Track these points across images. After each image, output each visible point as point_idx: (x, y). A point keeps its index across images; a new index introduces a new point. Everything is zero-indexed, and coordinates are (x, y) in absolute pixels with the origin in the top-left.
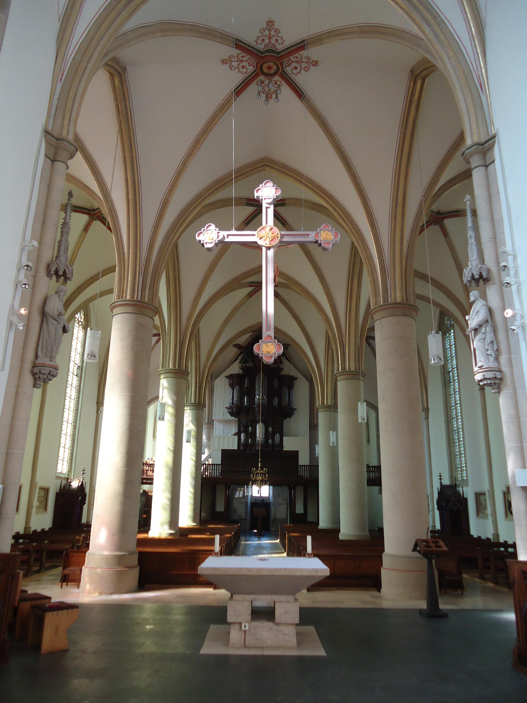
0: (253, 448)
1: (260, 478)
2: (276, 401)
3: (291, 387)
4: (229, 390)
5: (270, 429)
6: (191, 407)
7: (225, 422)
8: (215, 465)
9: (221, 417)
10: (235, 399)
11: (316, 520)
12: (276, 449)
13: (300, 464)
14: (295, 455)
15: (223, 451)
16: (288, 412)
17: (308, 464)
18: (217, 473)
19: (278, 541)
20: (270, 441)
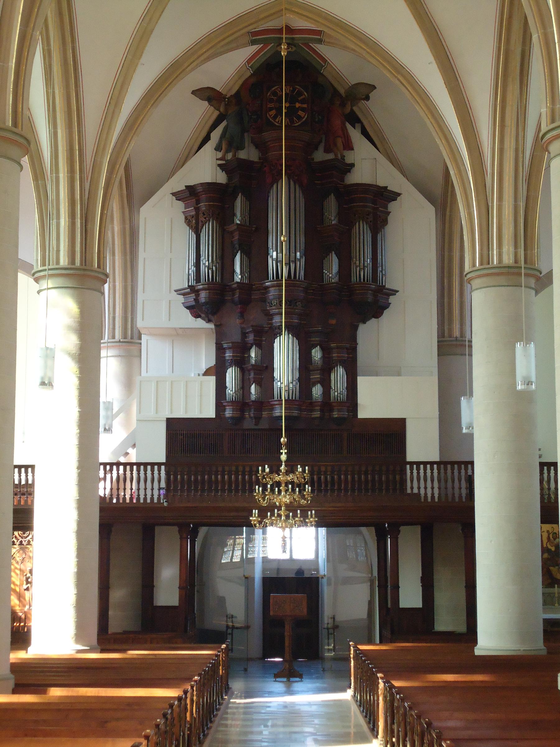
0: (265, 414)
1: (286, 499)
2: (332, 268)
3: (378, 223)
4: (184, 236)
5: (317, 354)
6: (59, 281)
7: (178, 335)
8: (145, 465)
9: (163, 322)
10: (205, 262)
11: (462, 628)
12: (335, 415)
14: (392, 433)
15: (171, 423)
16: (372, 300)
17: (437, 459)
18: (154, 490)
19: (348, 695)
20: (317, 391)
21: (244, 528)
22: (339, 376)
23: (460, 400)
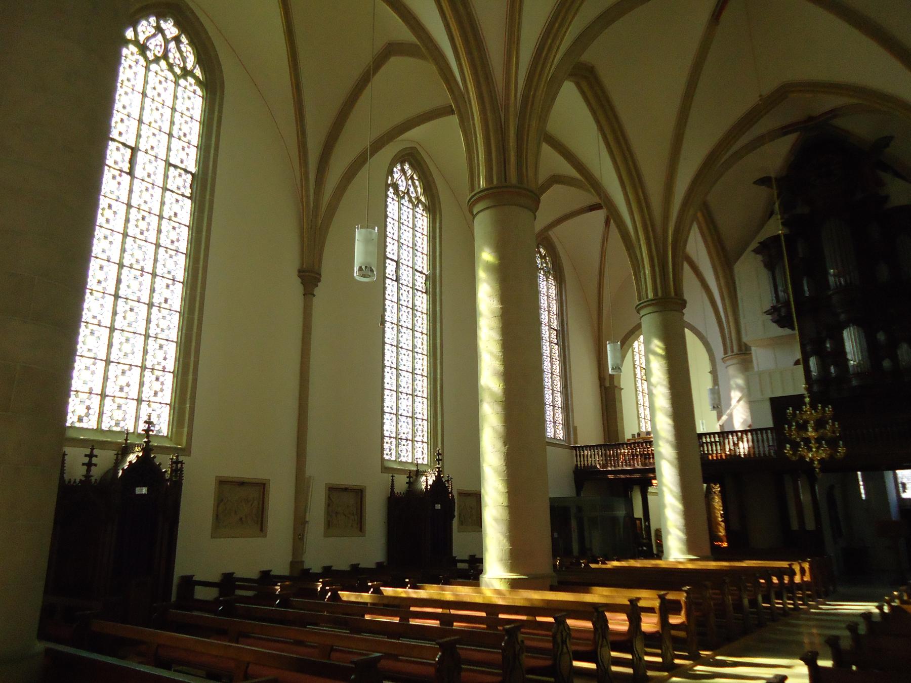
4: (764, 276)
20: (886, 364)
21: (859, 473)
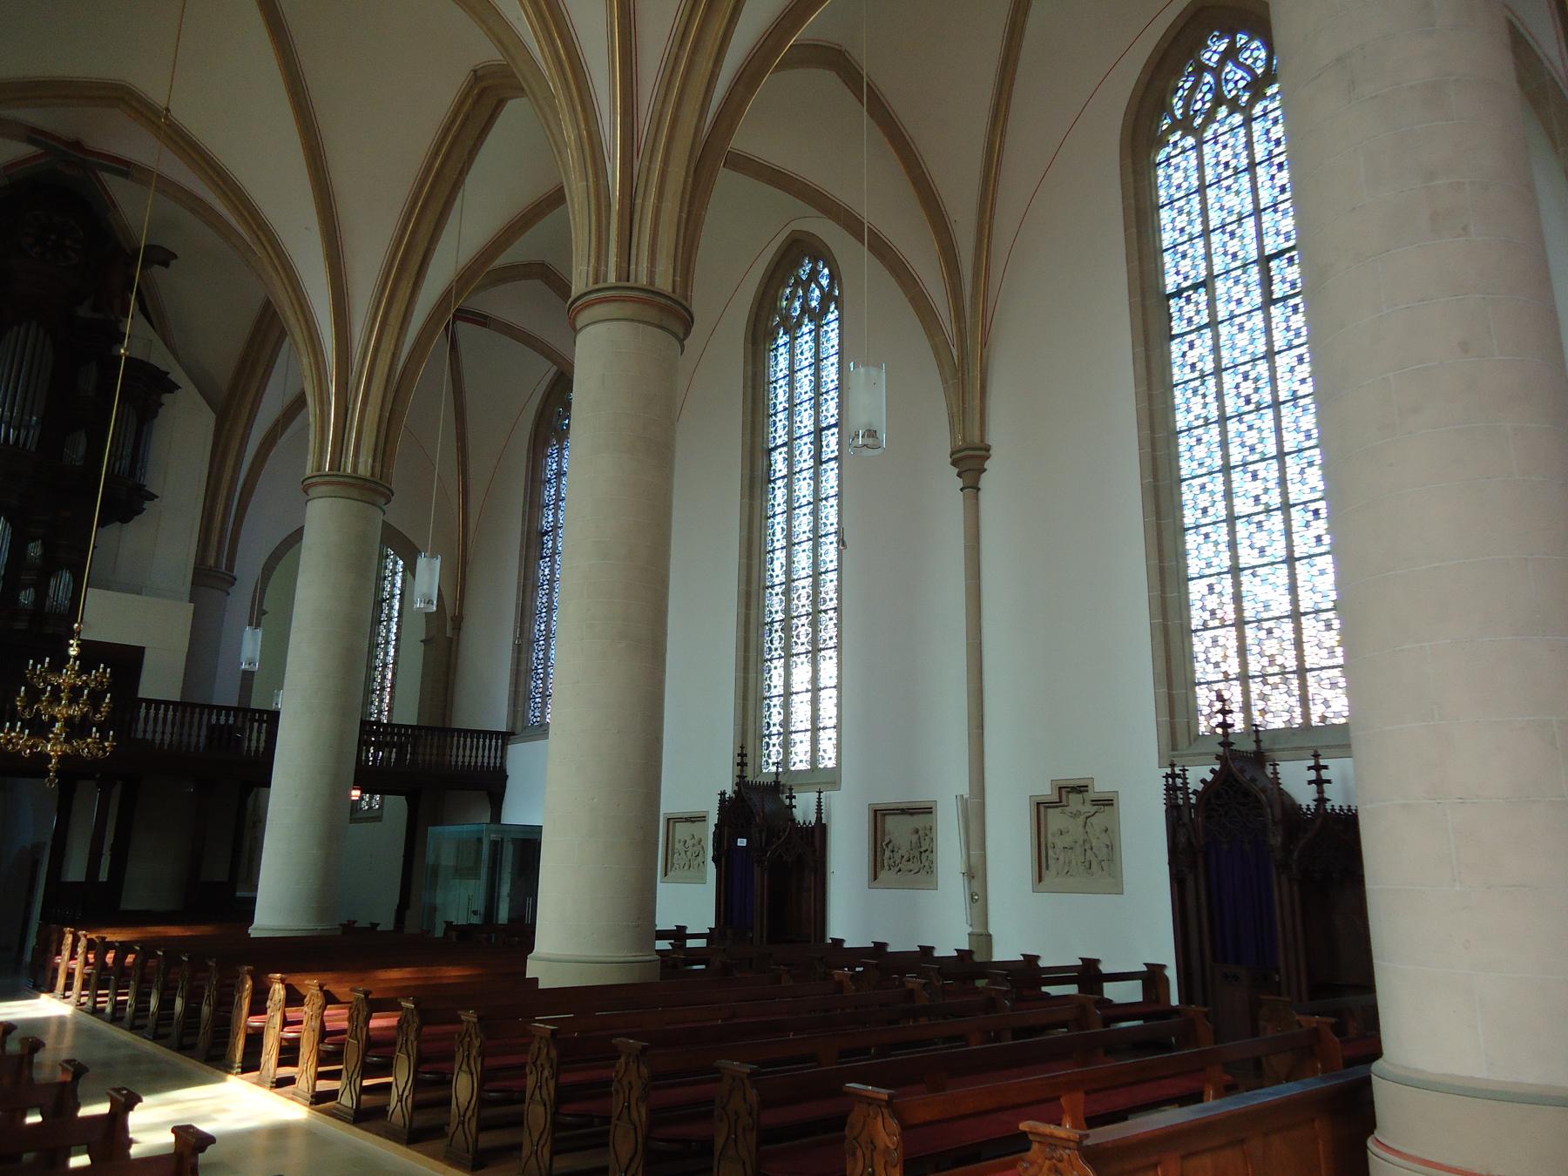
5: (35, 550)
13: (141, 695)
20: (26, 597)
22: (61, 585)
23: (242, 631)
